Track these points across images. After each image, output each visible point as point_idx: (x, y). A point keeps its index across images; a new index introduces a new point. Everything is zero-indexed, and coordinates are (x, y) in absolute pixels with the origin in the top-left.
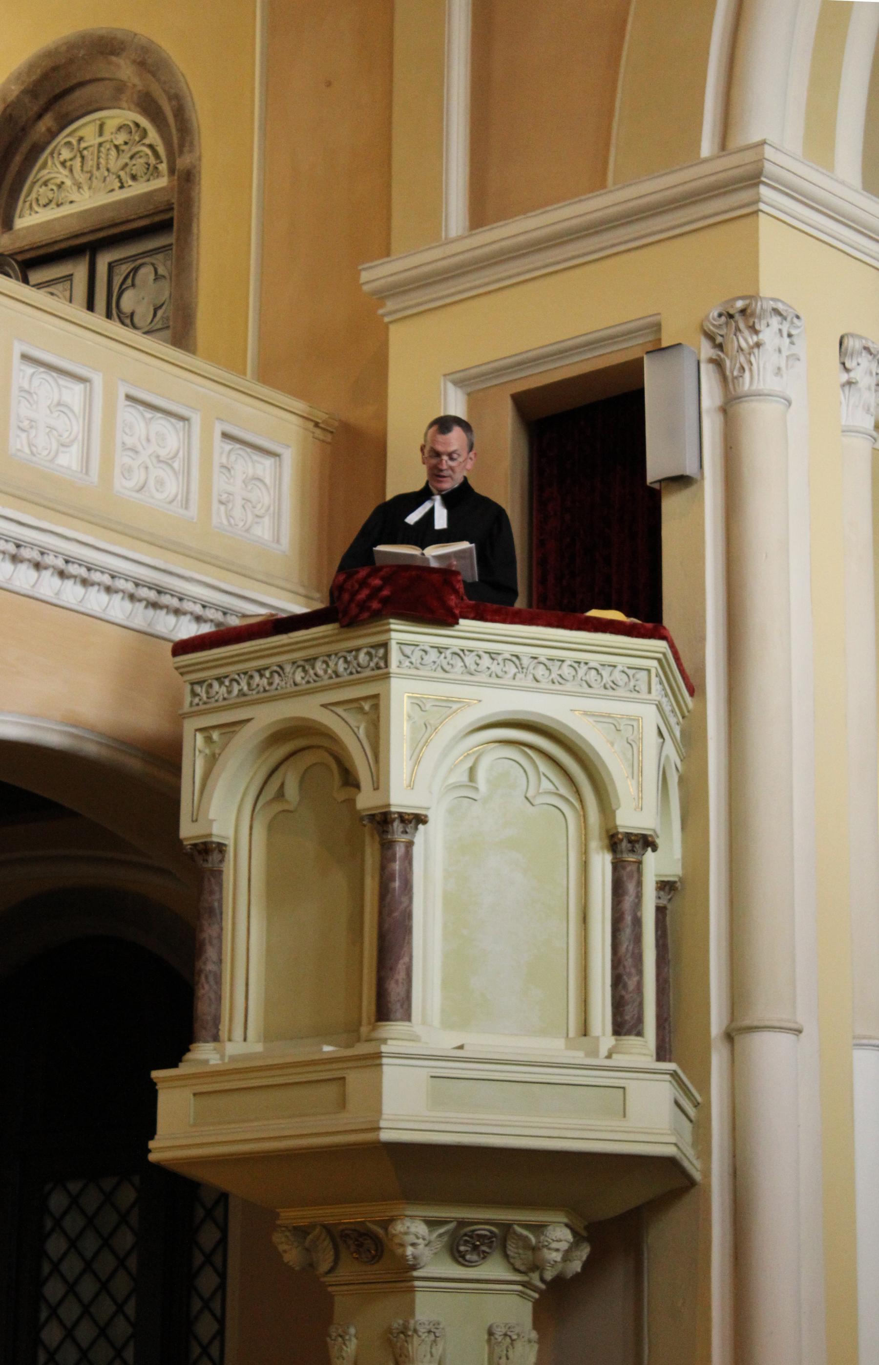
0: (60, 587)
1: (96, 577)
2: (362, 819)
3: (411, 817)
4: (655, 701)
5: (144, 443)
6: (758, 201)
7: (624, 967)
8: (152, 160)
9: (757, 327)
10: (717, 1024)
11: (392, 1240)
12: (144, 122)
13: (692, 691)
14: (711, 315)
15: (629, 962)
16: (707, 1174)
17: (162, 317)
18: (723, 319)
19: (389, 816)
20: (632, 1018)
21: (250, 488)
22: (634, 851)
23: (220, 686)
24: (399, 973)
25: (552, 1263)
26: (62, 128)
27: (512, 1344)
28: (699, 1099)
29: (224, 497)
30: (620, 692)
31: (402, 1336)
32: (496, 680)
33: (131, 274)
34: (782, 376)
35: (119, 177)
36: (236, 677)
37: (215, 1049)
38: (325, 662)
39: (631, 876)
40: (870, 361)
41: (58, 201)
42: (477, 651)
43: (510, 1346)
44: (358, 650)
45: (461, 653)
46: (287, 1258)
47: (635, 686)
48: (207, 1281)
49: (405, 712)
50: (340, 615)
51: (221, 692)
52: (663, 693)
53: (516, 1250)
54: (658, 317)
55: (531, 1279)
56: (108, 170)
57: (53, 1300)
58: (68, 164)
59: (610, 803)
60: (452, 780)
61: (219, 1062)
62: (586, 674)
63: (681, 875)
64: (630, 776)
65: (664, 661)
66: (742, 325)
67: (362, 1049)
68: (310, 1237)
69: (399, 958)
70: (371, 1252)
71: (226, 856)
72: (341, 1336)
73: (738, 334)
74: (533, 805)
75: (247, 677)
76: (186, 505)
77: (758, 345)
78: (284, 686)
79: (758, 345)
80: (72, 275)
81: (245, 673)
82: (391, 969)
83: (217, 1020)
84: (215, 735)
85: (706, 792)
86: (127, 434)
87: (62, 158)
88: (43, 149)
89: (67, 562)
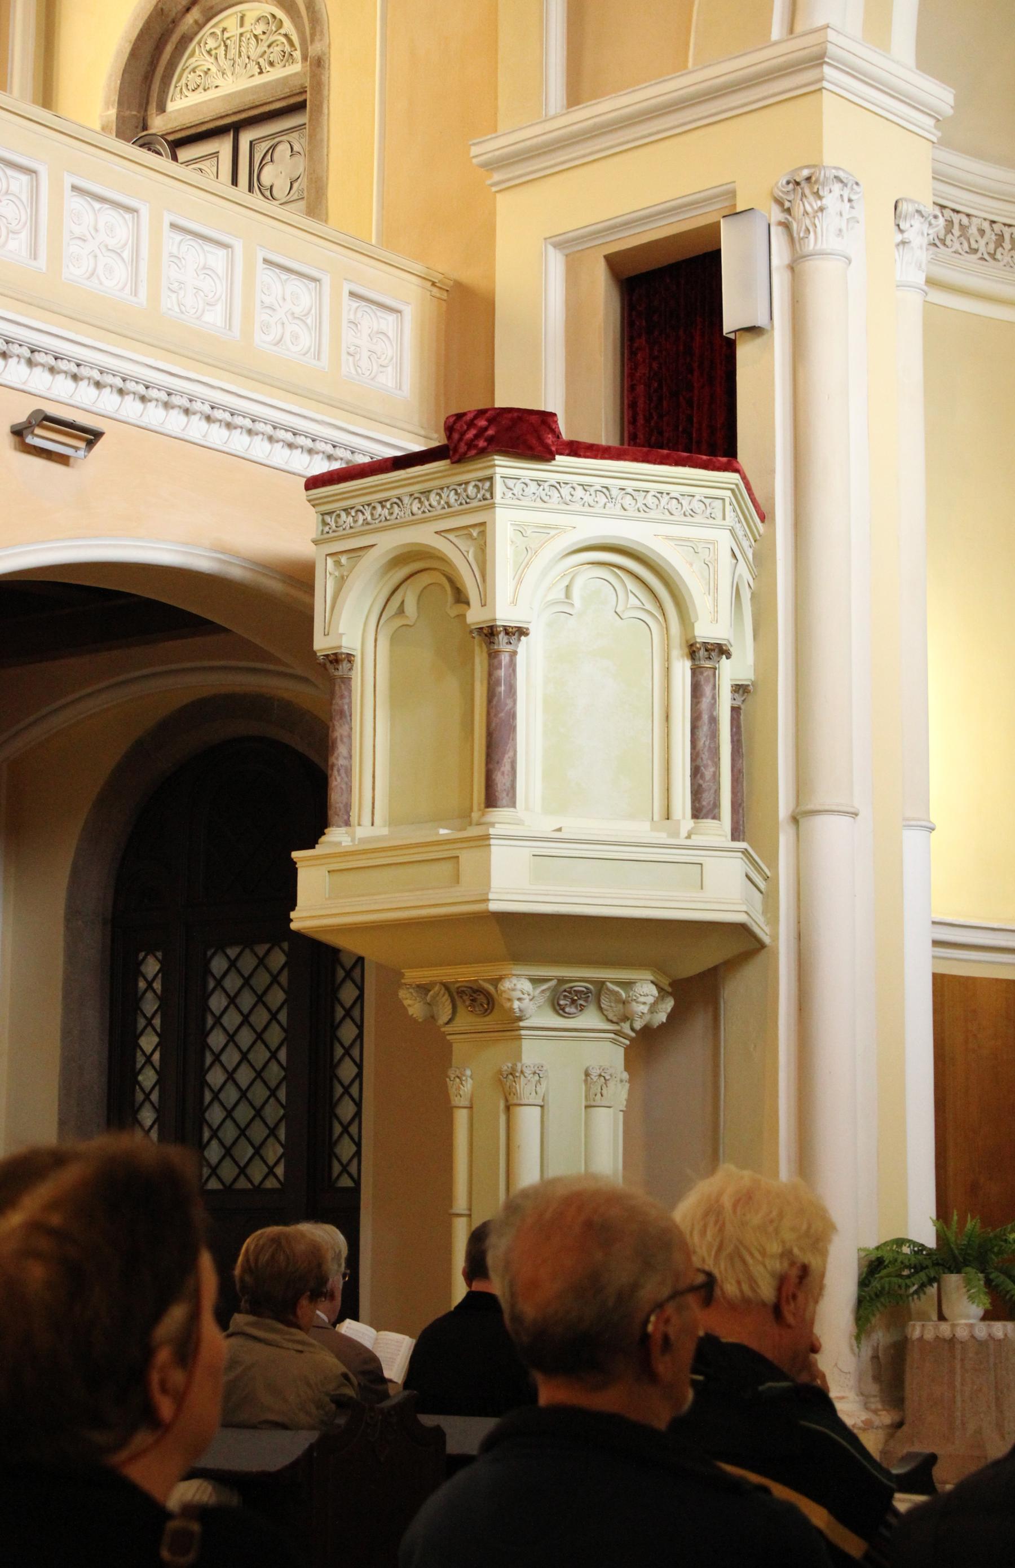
0: (208, 430)
1: (238, 421)
2: (471, 632)
3: (514, 630)
5: (281, 302)
6: (822, 79)
7: (702, 759)
8: (288, 48)
9: (821, 193)
10: (784, 808)
11: (501, 996)
12: (280, 14)
13: (762, 518)
14: (780, 183)
15: (705, 755)
16: (775, 937)
17: (298, 189)
18: (791, 186)
19: (495, 629)
20: (709, 804)
21: (375, 341)
22: (710, 659)
23: (347, 517)
24: (505, 766)
25: (640, 1014)
27: (606, 1083)
28: (769, 874)
29: (352, 350)
30: (697, 519)
31: (511, 1077)
33: (271, 151)
34: (843, 237)
35: (258, 63)
36: (361, 508)
37: (346, 833)
38: (438, 494)
39: (707, 680)
40: (922, 223)
41: (205, 87)
43: (605, 1086)
44: (467, 483)
45: (558, 486)
46: (411, 1011)
47: (711, 514)
48: (347, 1032)
49: (509, 536)
50: (451, 453)
51: (348, 522)
52: (737, 519)
53: (609, 1004)
54: (732, 185)
55: (622, 1027)
56: (249, 58)
57: (217, 1049)
58: (213, 52)
59: (689, 619)
60: (550, 597)
61: (351, 844)
62: (668, 504)
63: (753, 679)
64: (707, 593)
66: (807, 191)
67: (473, 832)
68: (431, 993)
69: (504, 754)
70: (483, 1007)
71: (355, 665)
72: (458, 1077)
73: (804, 199)
74: (622, 619)
75: (370, 508)
76: (318, 356)
77: (821, 209)
78: (403, 516)
79: (821, 209)
80: (218, 152)
81: (368, 505)
82: (498, 763)
83: (348, 807)
84: (343, 559)
85: (776, 604)
86: (265, 294)
87: (208, 48)
88: (191, 39)
89: (213, 408)
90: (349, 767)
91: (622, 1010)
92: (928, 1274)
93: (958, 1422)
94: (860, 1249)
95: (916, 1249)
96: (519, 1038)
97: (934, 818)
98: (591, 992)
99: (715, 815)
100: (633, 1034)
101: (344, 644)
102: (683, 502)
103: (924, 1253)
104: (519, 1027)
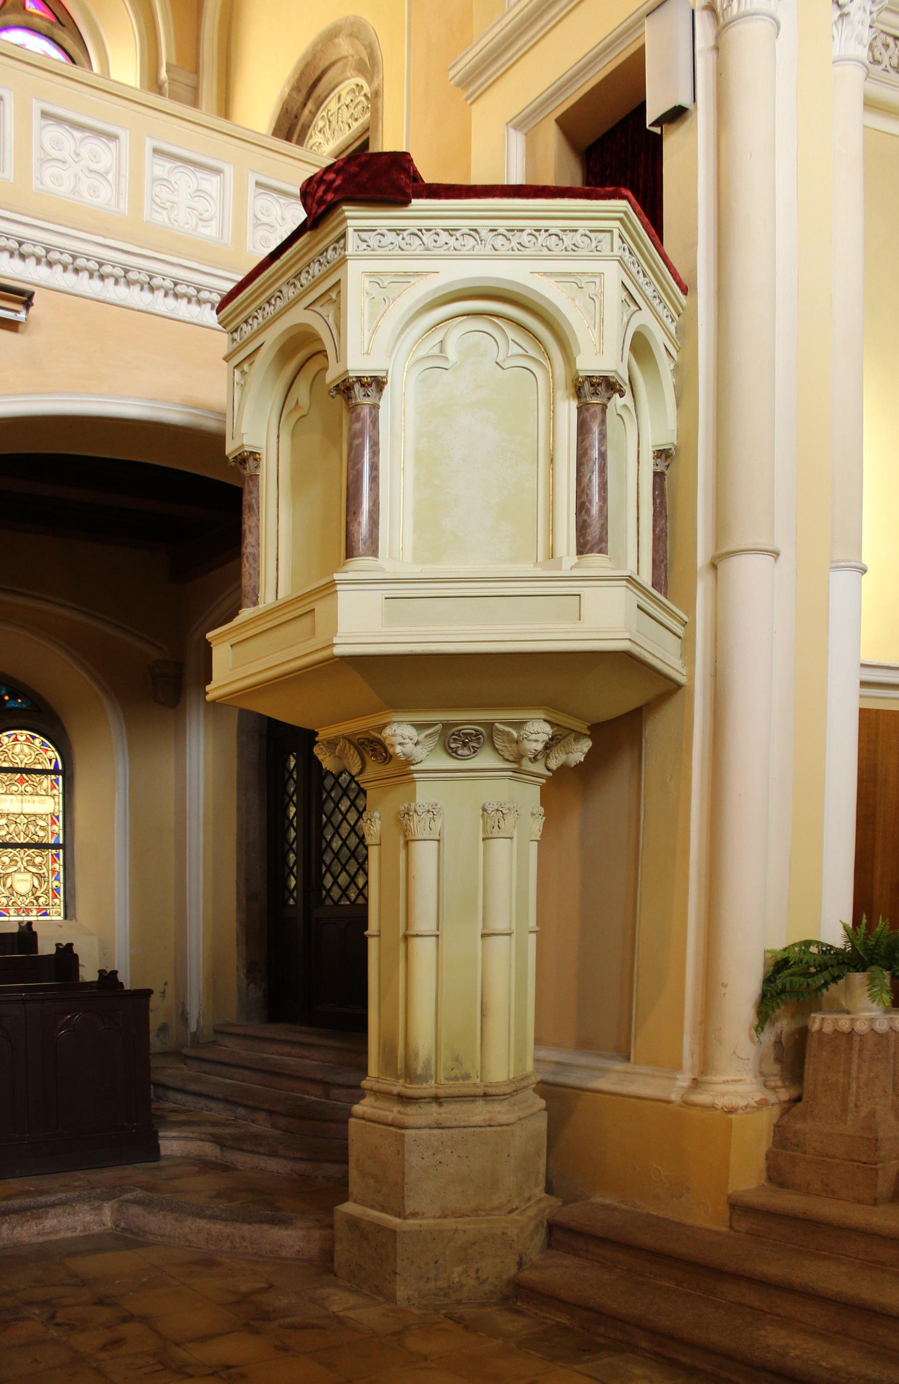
4: (616, 256)
5: (281, 222)
10: (702, 558)
13: (685, 291)
16: (691, 676)
22: (598, 394)
26: (318, 108)
28: (686, 618)
32: (456, 255)
36: (256, 313)
39: (594, 416)
42: (435, 229)
43: (502, 819)
45: (420, 234)
47: (597, 247)
53: (503, 744)
60: (422, 352)
65: (625, 219)
68: (338, 747)
70: (383, 755)
88: (309, 127)
90: (257, 554)
91: (516, 750)
92: (832, 974)
93: (851, 1105)
94: (768, 951)
95: (824, 949)
96: (413, 781)
97: (866, 560)
98: (481, 734)
99: (601, 549)
100: (550, 774)
101: (245, 442)
102: (564, 237)
103: (832, 952)
104: (411, 770)
